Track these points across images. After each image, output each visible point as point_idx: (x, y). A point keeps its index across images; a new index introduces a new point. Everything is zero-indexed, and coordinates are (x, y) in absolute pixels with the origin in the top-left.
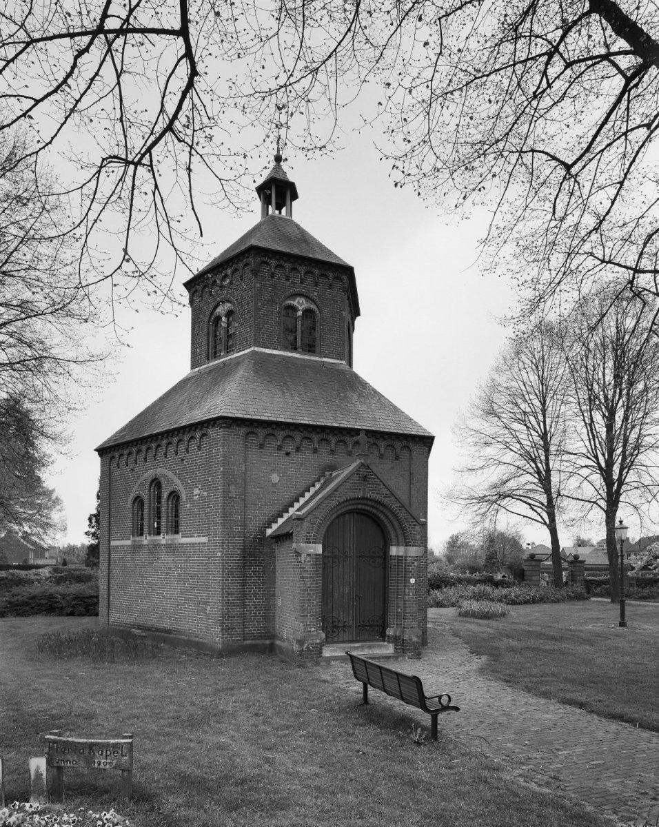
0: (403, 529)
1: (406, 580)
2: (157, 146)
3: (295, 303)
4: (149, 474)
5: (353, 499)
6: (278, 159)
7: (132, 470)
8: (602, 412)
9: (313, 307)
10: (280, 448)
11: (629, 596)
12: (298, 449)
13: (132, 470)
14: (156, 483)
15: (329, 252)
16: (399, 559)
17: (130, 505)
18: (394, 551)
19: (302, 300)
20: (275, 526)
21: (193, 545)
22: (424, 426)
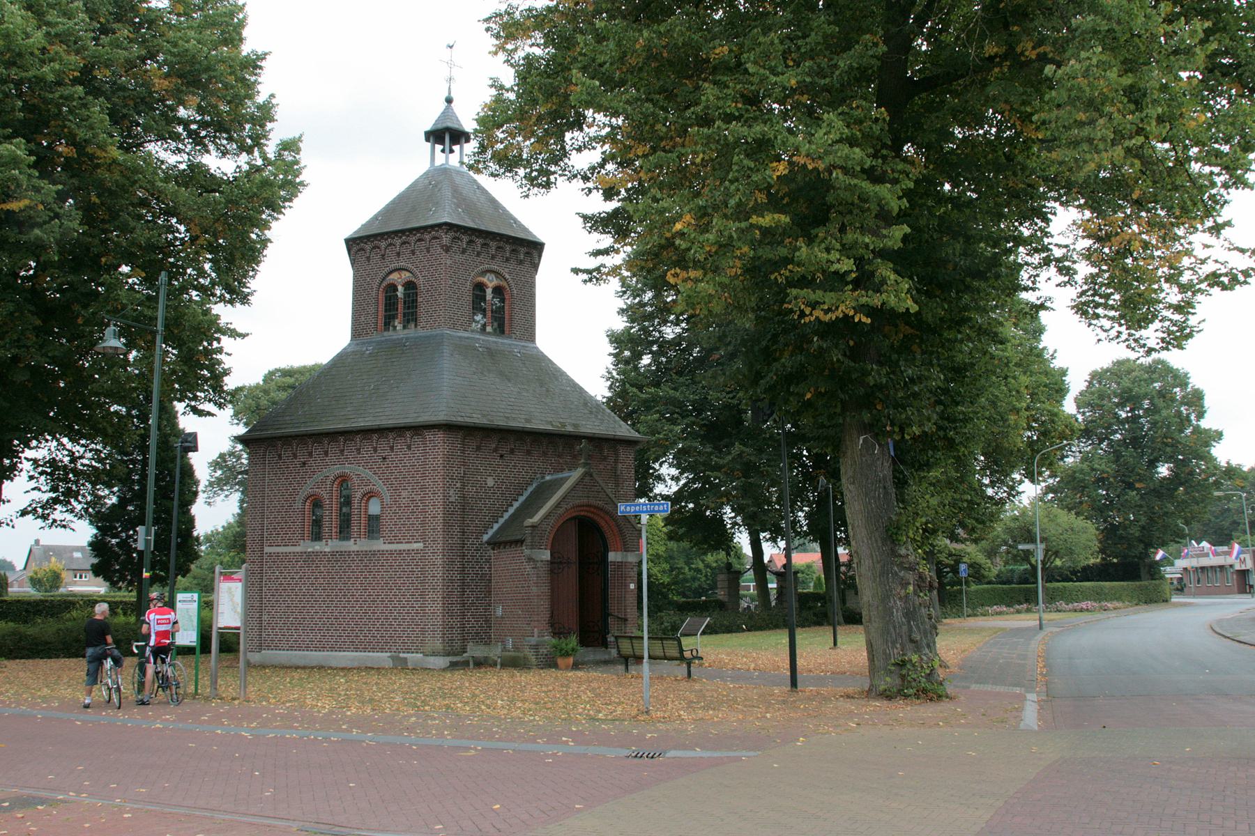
0: (620, 531)
1: (627, 586)
2: (798, 657)
3: (485, 280)
4: (336, 470)
5: (579, 506)
6: (449, 101)
7: (304, 464)
8: (1105, 316)
9: (504, 284)
10: (495, 450)
11: (839, 624)
12: (512, 452)
13: (304, 464)
14: (343, 480)
15: (525, 230)
16: (620, 565)
17: (298, 505)
18: (613, 556)
19: (492, 276)
20: (491, 532)
21: (400, 552)
22: (535, 233)
